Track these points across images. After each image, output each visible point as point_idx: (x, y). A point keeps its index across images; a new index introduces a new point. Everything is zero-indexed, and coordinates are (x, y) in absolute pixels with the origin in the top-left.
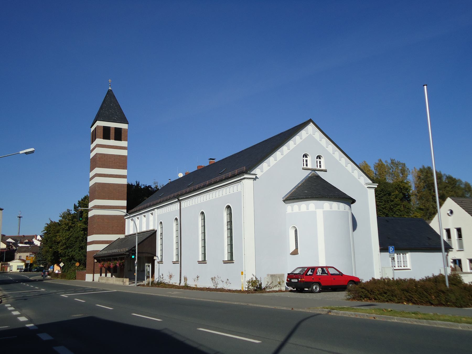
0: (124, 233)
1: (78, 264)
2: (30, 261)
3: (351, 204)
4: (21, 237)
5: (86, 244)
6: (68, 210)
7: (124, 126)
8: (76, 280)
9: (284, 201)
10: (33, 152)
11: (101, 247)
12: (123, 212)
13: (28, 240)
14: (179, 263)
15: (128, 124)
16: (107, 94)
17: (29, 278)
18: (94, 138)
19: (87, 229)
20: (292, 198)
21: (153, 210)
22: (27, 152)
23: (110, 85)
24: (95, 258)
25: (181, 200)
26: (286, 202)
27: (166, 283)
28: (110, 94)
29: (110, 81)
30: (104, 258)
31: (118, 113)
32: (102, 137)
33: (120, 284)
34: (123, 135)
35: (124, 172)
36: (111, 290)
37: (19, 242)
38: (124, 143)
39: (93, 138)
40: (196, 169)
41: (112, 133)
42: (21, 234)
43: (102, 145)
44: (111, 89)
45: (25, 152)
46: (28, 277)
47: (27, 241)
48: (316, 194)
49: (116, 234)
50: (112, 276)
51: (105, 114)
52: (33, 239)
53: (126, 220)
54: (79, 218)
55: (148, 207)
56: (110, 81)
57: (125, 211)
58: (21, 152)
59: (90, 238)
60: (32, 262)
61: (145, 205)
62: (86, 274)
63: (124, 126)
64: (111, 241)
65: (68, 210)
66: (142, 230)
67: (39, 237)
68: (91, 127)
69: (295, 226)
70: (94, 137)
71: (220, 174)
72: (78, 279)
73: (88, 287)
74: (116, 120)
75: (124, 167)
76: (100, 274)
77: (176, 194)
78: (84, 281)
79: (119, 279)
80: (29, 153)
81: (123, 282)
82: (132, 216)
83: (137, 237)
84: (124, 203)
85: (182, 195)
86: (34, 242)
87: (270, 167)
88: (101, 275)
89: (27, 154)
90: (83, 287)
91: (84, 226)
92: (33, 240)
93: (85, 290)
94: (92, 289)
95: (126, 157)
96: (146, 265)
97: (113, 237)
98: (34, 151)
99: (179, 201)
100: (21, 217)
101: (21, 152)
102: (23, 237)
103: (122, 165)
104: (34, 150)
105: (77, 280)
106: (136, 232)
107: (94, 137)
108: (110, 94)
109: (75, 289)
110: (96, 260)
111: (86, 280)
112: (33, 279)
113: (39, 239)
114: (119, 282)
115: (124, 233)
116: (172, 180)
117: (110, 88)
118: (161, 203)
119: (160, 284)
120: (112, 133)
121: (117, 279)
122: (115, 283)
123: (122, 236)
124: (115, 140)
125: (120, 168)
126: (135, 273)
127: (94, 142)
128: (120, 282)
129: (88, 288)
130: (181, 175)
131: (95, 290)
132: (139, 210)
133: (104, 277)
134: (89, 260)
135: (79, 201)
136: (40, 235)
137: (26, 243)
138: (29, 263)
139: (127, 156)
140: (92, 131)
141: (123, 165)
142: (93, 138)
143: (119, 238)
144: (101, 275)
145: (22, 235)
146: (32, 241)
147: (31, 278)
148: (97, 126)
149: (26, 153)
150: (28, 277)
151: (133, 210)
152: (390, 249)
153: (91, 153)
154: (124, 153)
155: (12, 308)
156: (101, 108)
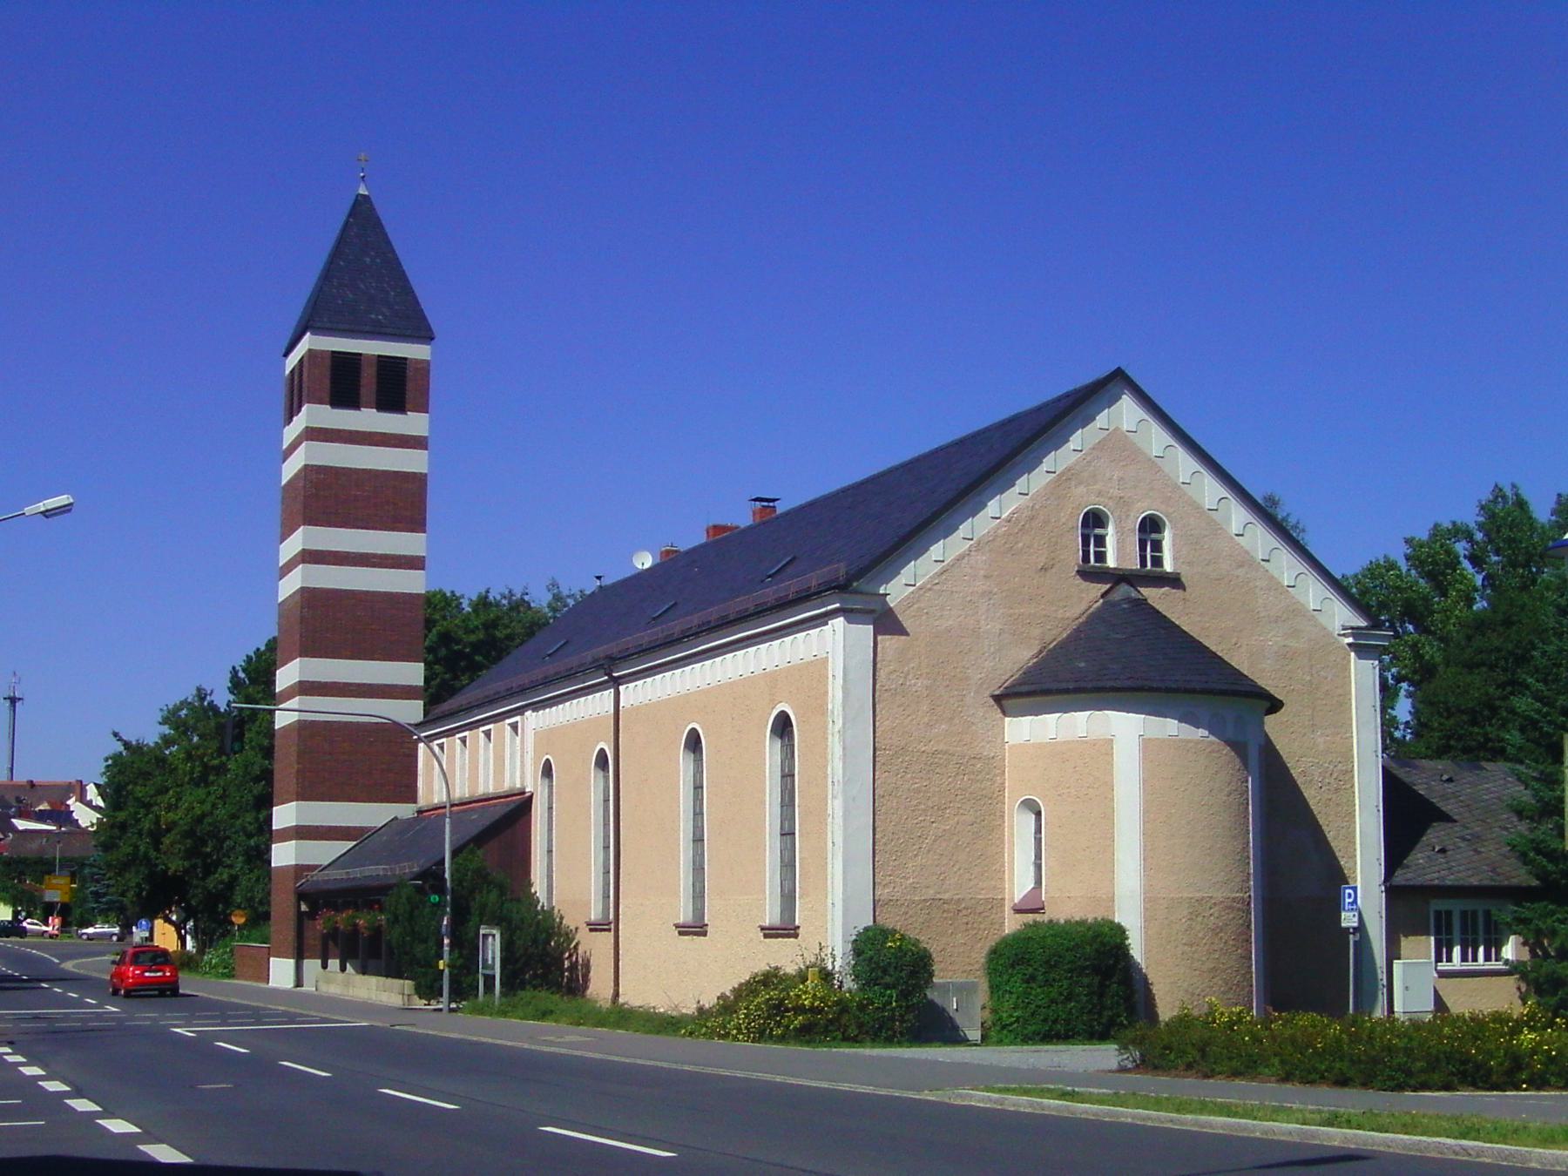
0: (413, 798)
2: (59, 892)
3: (1266, 715)
4: (20, 787)
6: (201, 694)
9: (998, 699)
10: (69, 511)
11: (325, 852)
12: (410, 711)
13: (49, 803)
14: (609, 930)
16: (350, 215)
17: (59, 964)
18: (295, 406)
19: (271, 772)
20: (1025, 688)
21: (520, 711)
22: (47, 511)
23: (362, 174)
25: (619, 677)
26: (1006, 703)
27: (640, 1007)
28: (362, 215)
31: (392, 293)
32: (327, 398)
33: (391, 1001)
36: (352, 1021)
37: (13, 810)
38: (412, 423)
39: (292, 404)
40: (702, 539)
41: (368, 376)
42: (21, 777)
43: (326, 430)
44: (366, 193)
45: (42, 509)
46: (57, 961)
47: (44, 806)
48: (1116, 677)
49: (382, 801)
50: (343, 969)
51: (340, 302)
52: (70, 798)
54: (232, 743)
55: (512, 695)
57: (418, 705)
58: (28, 510)
59: (284, 815)
60: (66, 899)
61: (500, 686)
65: (199, 689)
67: (92, 793)
68: (286, 355)
69: (1024, 798)
70: (296, 399)
71: (770, 576)
73: (273, 1007)
76: (319, 961)
77: (601, 651)
78: (263, 985)
79: (390, 980)
80: (53, 512)
81: (401, 996)
82: (426, 737)
83: (448, 820)
84: (412, 673)
85: (625, 657)
86: (74, 814)
87: (943, 564)
88: (325, 966)
89: (47, 517)
90: (253, 1007)
91: (259, 762)
92: (69, 802)
93: (257, 1015)
94: (285, 1014)
96: (482, 932)
97: (373, 814)
98: (71, 504)
99: (616, 682)
100: (20, 699)
101: (28, 510)
102: (28, 787)
104: (72, 501)
105: (237, 979)
106: (445, 800)
107: (296, 399)
108: (362, 215)
109: (223, 1012)
110: (305, 904)
111: (272, 984)
112: (74, 967)
113: (91, 801)
114: (386, 993)
115: (414, 800)
116: (607, 581)
117: (363, 191)
118: (548, 683)
119: (622, 1016)
120: (368, 376)
121: (381, 983)
122: (374, 998)
123: (405, 811)
125: (398, 525)
126: (442, 958)
127: (295, 419)
128: (393, 994)
129: (271, 1010)
130: (644, 561)
131: (292, 1018)
132: (469, 709)
133: (336, 972)
134: (283, 905)
135: (247, 656)
136: (95, 784)
137: (41, 816)
138: (57, 903)
140: (287, 372)
142: (292, 404)
143: (396, 818)
144: (325, 966)
145: (25, 780)
146: (63, 808)
147: (69, 966)
149: (46, 514)
150: (57, 961)
151: (446, 707)
152: (1344, 905)
153: (284, 461)
155: (19, 1059)
156: (327, 275)
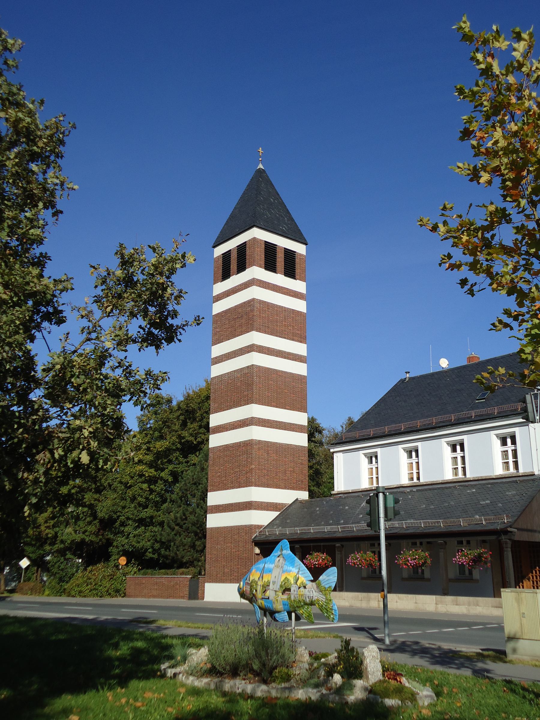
1: (124, 560)
5: (205, 510)
7: (299, 248)
8: (124, 598)
15: (306, 244)
23: (260, 159)
24: (257, 543)
29: (260, 150)
30: (308, 544)
32: (263, 262)
34: (297, 266)
35: (301, 349)
38: (299, 286)
40: (465, 363)
53: (335, 455)
56: (260, 150)
62: (207, 585)
63: (299, 248)
64: (282, 505)
66: (493, 471)
72: (130, 596)
74: (284, 232)
75: (301, 339)
95: (304, 316)
103: (297, 332)
117: (261, 166)
124: (285, 275)
139: (305, 314)
141: (299, 332)
148: (255, 238)
154: (300, 306)
